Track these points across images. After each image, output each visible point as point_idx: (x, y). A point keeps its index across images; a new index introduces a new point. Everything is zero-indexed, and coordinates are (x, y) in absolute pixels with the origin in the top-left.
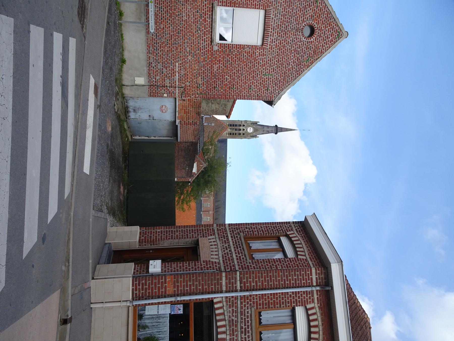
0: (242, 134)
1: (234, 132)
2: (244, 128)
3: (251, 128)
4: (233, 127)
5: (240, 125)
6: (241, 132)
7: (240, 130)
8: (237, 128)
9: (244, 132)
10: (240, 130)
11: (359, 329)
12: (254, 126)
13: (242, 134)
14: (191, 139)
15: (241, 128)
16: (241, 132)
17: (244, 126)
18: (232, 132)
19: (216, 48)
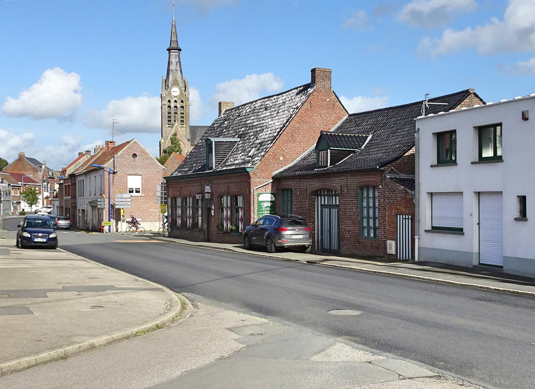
0: (170, 119)
1: (179, 116)
2: (172, 101)
3: (172, 90)
4: (173, 117)
5: (169, 107)
6: (179, 106)
7: (176, 107)
8: (172, 112)
9: (180, 101)
10: (176, 107)
11: (244, 120)
12: (170, 86)
13: (170, 119)
14: (269, 203)
15: (173, 105)
16: (179, 106)
17: (169, 101)
18: (180, 119)
19: (143, 195)
